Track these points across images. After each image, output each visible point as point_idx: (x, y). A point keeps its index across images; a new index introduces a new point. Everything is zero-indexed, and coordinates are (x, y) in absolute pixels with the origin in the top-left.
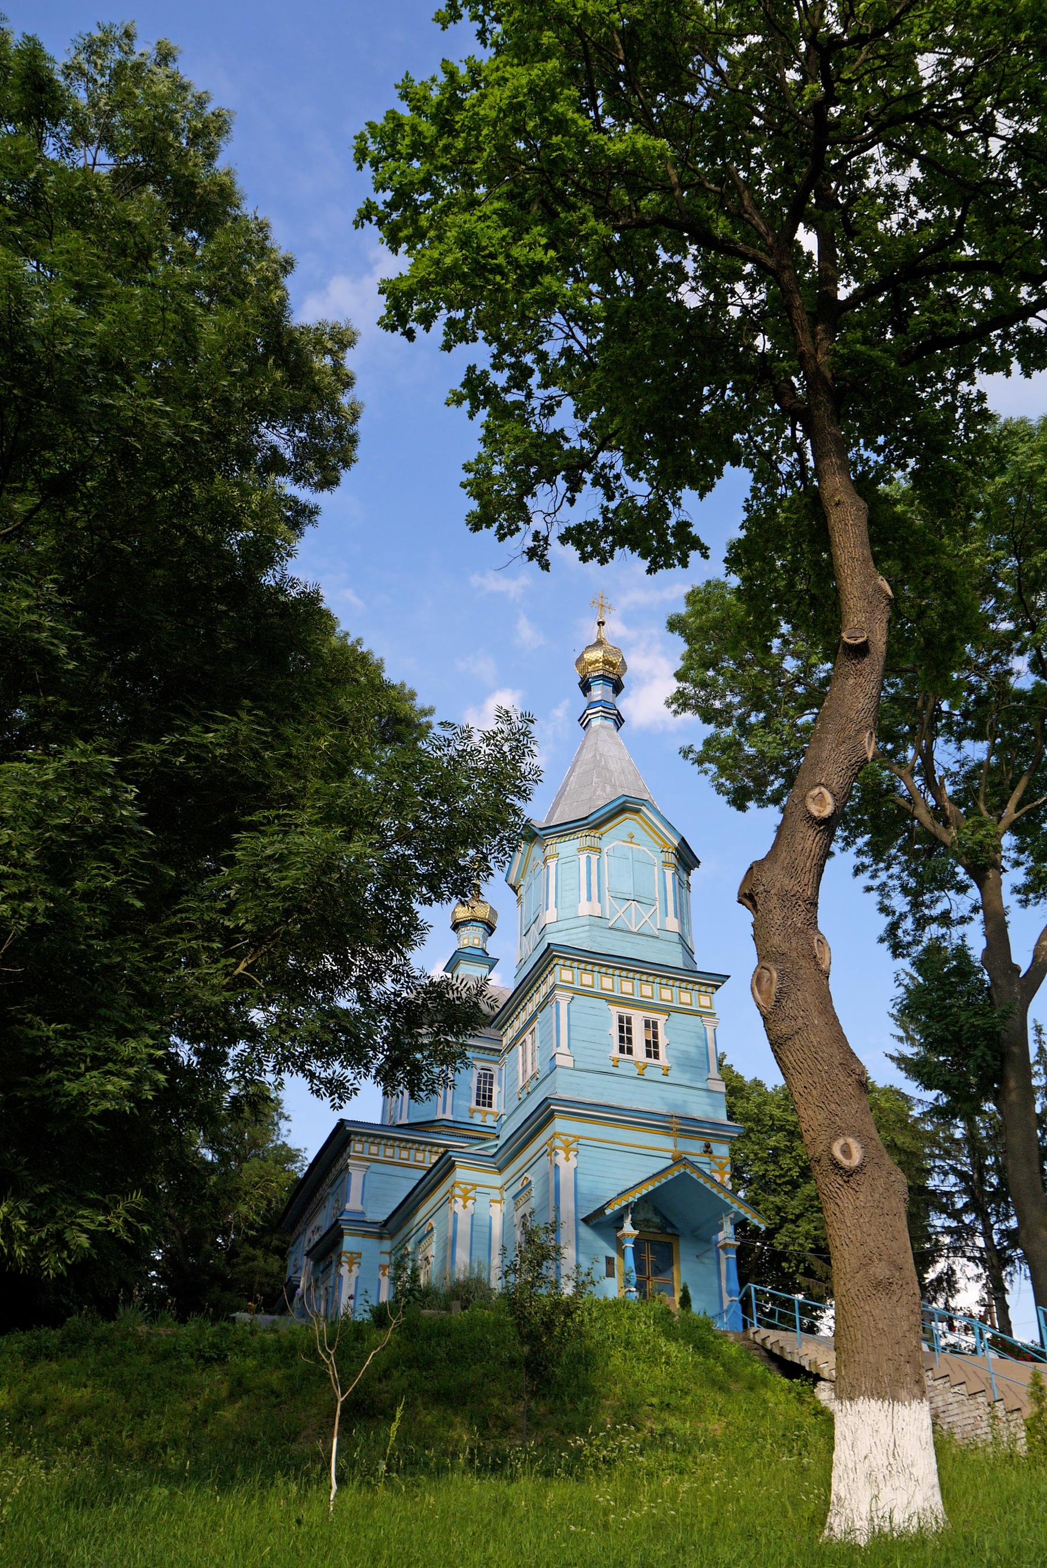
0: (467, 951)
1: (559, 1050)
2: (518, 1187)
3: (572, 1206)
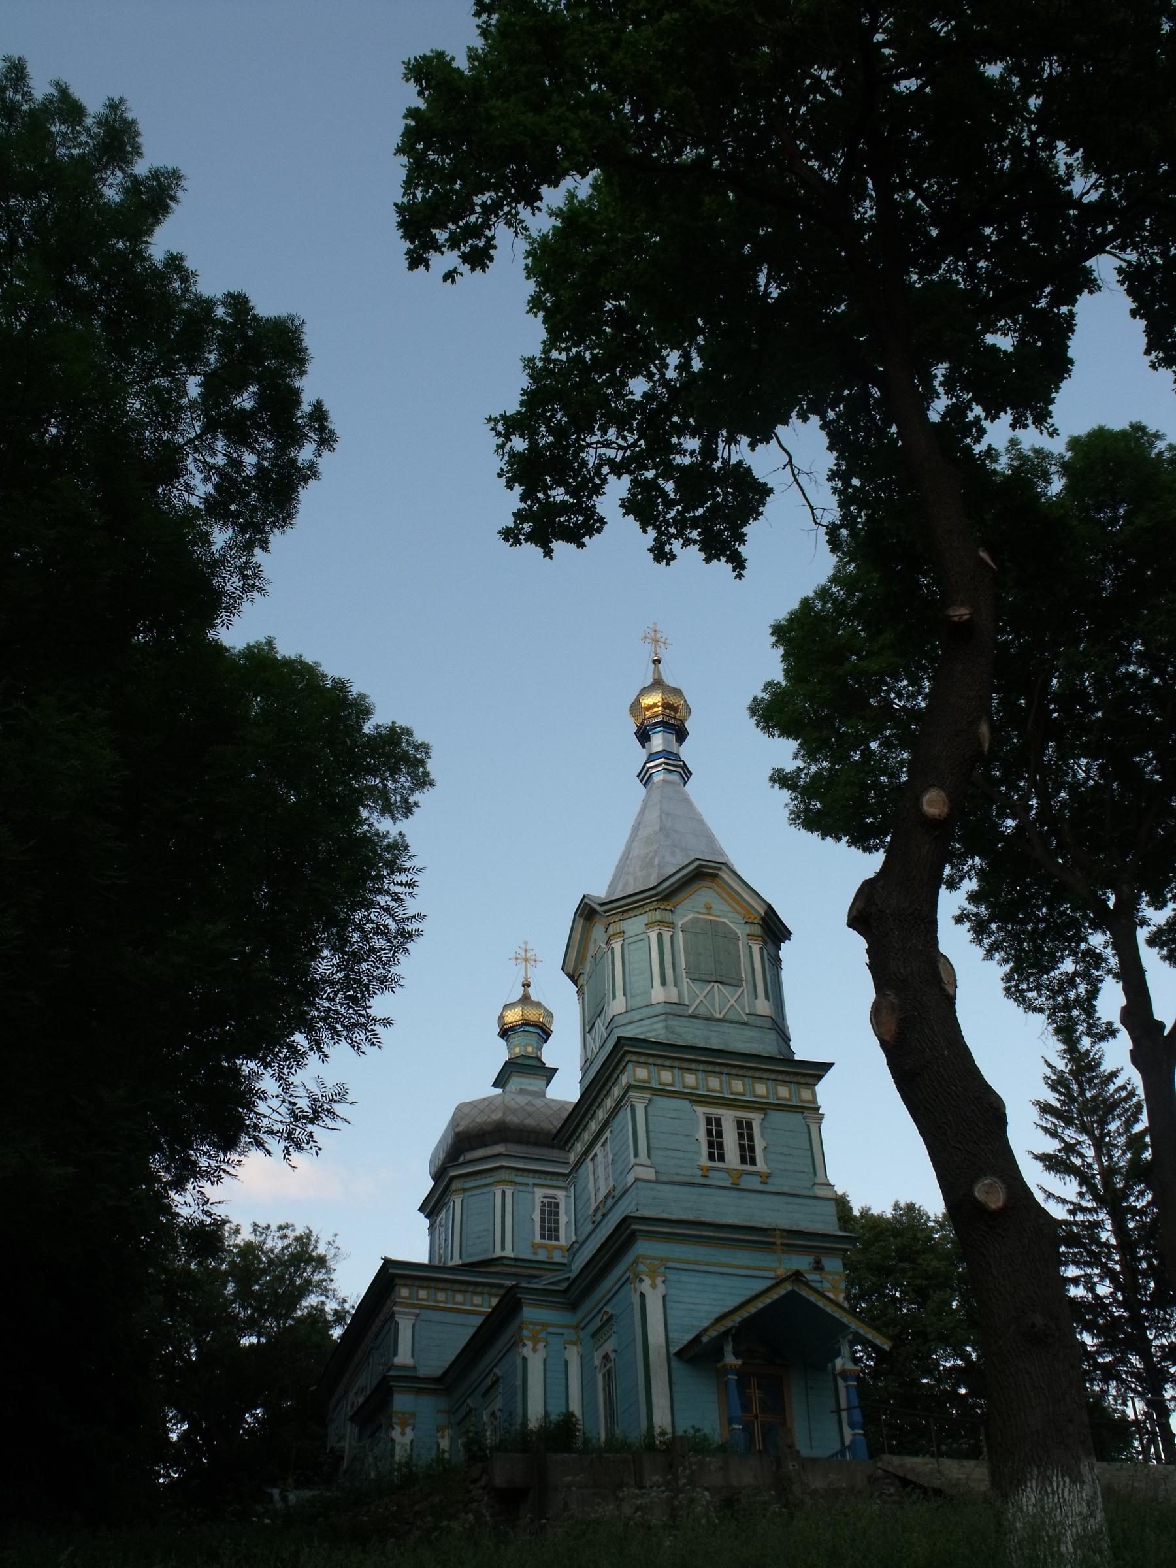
0: (519, 1061)
1: (638, 1161)
2: (597, 1323)
3: (662, 1339)
